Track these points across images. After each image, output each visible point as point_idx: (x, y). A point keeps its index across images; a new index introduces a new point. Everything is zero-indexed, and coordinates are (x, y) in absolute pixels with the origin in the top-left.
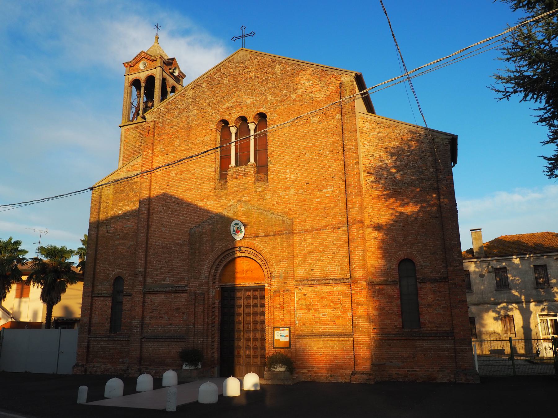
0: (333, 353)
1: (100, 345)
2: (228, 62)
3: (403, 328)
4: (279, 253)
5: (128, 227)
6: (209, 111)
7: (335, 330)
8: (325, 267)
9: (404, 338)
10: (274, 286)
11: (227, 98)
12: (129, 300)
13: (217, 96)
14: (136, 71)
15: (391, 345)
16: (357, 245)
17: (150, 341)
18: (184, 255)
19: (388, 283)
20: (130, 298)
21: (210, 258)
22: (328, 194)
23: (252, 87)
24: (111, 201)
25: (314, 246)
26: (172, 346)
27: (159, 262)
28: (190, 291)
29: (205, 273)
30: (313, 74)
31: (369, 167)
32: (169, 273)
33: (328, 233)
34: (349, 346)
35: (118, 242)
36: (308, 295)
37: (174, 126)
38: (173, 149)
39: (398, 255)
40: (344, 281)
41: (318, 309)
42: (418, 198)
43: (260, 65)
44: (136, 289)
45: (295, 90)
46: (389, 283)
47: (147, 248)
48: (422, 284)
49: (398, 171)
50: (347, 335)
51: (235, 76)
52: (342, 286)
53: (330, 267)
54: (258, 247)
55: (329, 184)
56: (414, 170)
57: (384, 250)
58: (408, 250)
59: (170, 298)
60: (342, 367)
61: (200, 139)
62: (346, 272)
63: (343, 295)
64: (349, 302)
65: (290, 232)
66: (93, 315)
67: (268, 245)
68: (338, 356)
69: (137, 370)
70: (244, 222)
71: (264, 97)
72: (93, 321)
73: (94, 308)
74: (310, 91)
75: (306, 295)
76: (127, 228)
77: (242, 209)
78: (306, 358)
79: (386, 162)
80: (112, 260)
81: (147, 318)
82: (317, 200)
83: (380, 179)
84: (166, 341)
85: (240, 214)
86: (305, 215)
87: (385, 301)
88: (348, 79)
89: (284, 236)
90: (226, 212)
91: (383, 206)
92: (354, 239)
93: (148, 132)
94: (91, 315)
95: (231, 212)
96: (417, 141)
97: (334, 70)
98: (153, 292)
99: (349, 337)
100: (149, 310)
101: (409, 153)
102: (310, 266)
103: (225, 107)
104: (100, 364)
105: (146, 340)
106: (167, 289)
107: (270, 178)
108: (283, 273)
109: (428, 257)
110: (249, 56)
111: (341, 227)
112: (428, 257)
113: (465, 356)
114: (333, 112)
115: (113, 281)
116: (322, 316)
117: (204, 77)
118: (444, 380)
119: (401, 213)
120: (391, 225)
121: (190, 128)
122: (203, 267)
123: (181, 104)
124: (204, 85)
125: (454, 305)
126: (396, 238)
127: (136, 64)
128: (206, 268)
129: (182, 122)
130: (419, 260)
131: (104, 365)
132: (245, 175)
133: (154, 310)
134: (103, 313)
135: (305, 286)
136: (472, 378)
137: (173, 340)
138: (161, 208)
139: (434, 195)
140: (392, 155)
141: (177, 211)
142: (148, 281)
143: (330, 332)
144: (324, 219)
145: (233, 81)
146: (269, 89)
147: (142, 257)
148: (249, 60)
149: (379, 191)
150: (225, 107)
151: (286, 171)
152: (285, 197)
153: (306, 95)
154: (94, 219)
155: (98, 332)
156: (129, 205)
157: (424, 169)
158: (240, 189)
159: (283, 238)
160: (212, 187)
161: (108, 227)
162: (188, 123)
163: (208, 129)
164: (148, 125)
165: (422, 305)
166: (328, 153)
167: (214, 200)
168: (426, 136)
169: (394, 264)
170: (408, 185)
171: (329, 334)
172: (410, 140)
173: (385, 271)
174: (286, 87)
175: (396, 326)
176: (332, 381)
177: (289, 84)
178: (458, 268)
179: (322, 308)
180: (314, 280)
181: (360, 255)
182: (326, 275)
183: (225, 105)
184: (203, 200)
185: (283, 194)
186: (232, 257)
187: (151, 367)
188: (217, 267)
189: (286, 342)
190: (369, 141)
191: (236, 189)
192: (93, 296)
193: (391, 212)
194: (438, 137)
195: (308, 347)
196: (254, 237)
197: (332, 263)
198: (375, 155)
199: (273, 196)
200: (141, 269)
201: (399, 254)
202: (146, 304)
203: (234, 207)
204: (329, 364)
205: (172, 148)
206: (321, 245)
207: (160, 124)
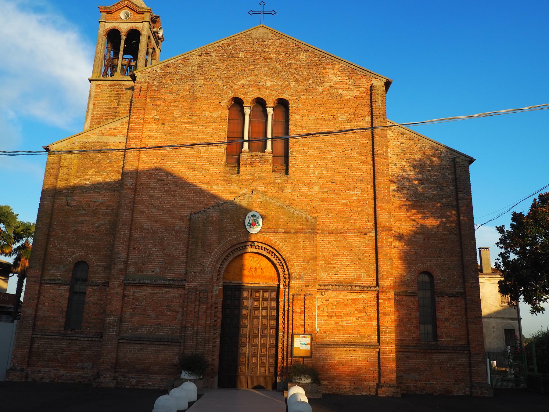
0: (356, 363)
1: (49, 344)
2: (245, 36)
4: (301, 252)
5: (98, 202)
6: (220, 84)
7: (359, 340)
8: (349, 273)
9: (422, 351)
10: (294, 288)
13: (231, 70)
15: (408, 357)
16: (386, 253)
17: (130, 343)
18: (181, 244)
19: (408, 294)
20: (97, 289)
22: (356, 196)
24: (75, 167)
26: (161, 350)
27: (147, 248)
28: (189, 286)
29: (209, 267)
30: (342, 70)
31: (392, 175)
32: (159, 263)
33: (354, 238)
34: (373, 357)
35: (82, 219)
36: (330, 300)
37: (174, 92)
39: (417, 267)
40: (371, 289)
41: (341, 316)
42: (438, 213)
43: (282, 47)
44: (114, 279)
45: (322, 82)
46: (409, 294)
48: (440, 297)
49: (420, 184)
50: (373, 345)
51: (253, 52)
52: (368, 294)
53: (355, 274)
54: (277, 244)
55: (357, 186)
56: (435, 186)
57: (404, 261)
58: (428, 263)
59: (159, 293)
60: (365, 379)
61: (207, 114)
62: (372, 279)
63: (368, 303)
64: (374, 311)
65: (313, 232)
66: (40, 306)
67: (287, 243)
68: (361, 368)
69: (112, 378)
70: (263, 215)
71: (287, 83)
72: (40, 313)
73: (42, 297)
74: (338, 87)
75: (328, 300)
76: (97, 203)
77: (258, 200)
78: (327, 369)
79: (409, 173)
80: (72, 240)
81: (127, 315)
82: (343, 201)
83: (402, 189)
84: (154, 344)
85: (255, 205)
87: (404, 312)
88: (379, 83)
89: (307, 235)
90: (239, 201)
91: (405, 216)
92: (383, 247)
93: (140, 94)
94: (37, 306)
95: (245, 201)
96: (439, 157)
97: (364, 72)
98: (137, 285)
99: (376, 347)
100: (130, 305)
101: (430, 168)
102: (334, 270)
103: (239, 83)
104: (47, 369)
105: (125, 341)
106: (158, 282)
107: (292, 171)
108: (305, 275)
109: (446, 272)
110: (270, 35)
111: (369, 232)
112: (446, 272)
113: (479, 370)
114: (362, 114)
115: (72, 266)
116: (346, 325)
117: (215, 45)
118: (460, 393)
119: (422, 225)
120: (412, 236)
121: (194, 99)
122: (207, 260)
123: (184, 69)
124: (214, 54)
125: (471, 320)
126: (415, 250)
127: (115, 11)
128: (211, 261)
129: (184, 90)
130: (438, 273)
131: (54, 370)
133: (137, 305)
134: (56, 304)
135: (329, 291)
136: (487, 392)
137: (162, 343)
138: (152, 185)
139: (454, 212)
140: (414, 167)
141: (173, 191)
142: (130, 270)
143: (354, 342)
144: (350, 222)
145: (251, 58)
146: (292, 75)
147: (125, 241)
148: (269, 39)
149: (401, 200)
150: (239, 83)
151: (309, 166)
152: (308, 193)
153: (334, 90)
154: (50, 185)
155: (46, 328)
156: (100, 176)
157: (444, 185)
158: (255, 177)
159: (305, 237)
160: (220, 171)
161: (68, 198)
162: (193, 93)
163: (217, 105)
164: (140, 85)
165: (440, 319)
167: (223, 185)
168: (447, 155)
169: (414, 276)
170: (429, 199)
171: (353, 344)
172: (432, 156)
173: (404, 282)
174: (311, 77)
175: (414, 338)
176: (356, 393)
177: (316, 75)
179: (346, 316)
181: (389, 263)
182: (351, 281)
183: (239, 81)
184: (208, 183)
185: (305, 190)
186: (242, 252)
187: (130, 375)
188: (223, 262)
189: (307, 350)
190: (392, 149)
191: (250, 177)
192: (42, 282)
193: (412, 223)
194: (459, 157)
196: (271, 232)
197: (358, 269)
198: (398, 165)
199: (294, 190)
200: (121, 254)
201: (419, 266)
202: (126, 298)
203: (249, 196)
204: (351, 376)
205: (170, 117)
206: (346, 249)
207: (154, 87)
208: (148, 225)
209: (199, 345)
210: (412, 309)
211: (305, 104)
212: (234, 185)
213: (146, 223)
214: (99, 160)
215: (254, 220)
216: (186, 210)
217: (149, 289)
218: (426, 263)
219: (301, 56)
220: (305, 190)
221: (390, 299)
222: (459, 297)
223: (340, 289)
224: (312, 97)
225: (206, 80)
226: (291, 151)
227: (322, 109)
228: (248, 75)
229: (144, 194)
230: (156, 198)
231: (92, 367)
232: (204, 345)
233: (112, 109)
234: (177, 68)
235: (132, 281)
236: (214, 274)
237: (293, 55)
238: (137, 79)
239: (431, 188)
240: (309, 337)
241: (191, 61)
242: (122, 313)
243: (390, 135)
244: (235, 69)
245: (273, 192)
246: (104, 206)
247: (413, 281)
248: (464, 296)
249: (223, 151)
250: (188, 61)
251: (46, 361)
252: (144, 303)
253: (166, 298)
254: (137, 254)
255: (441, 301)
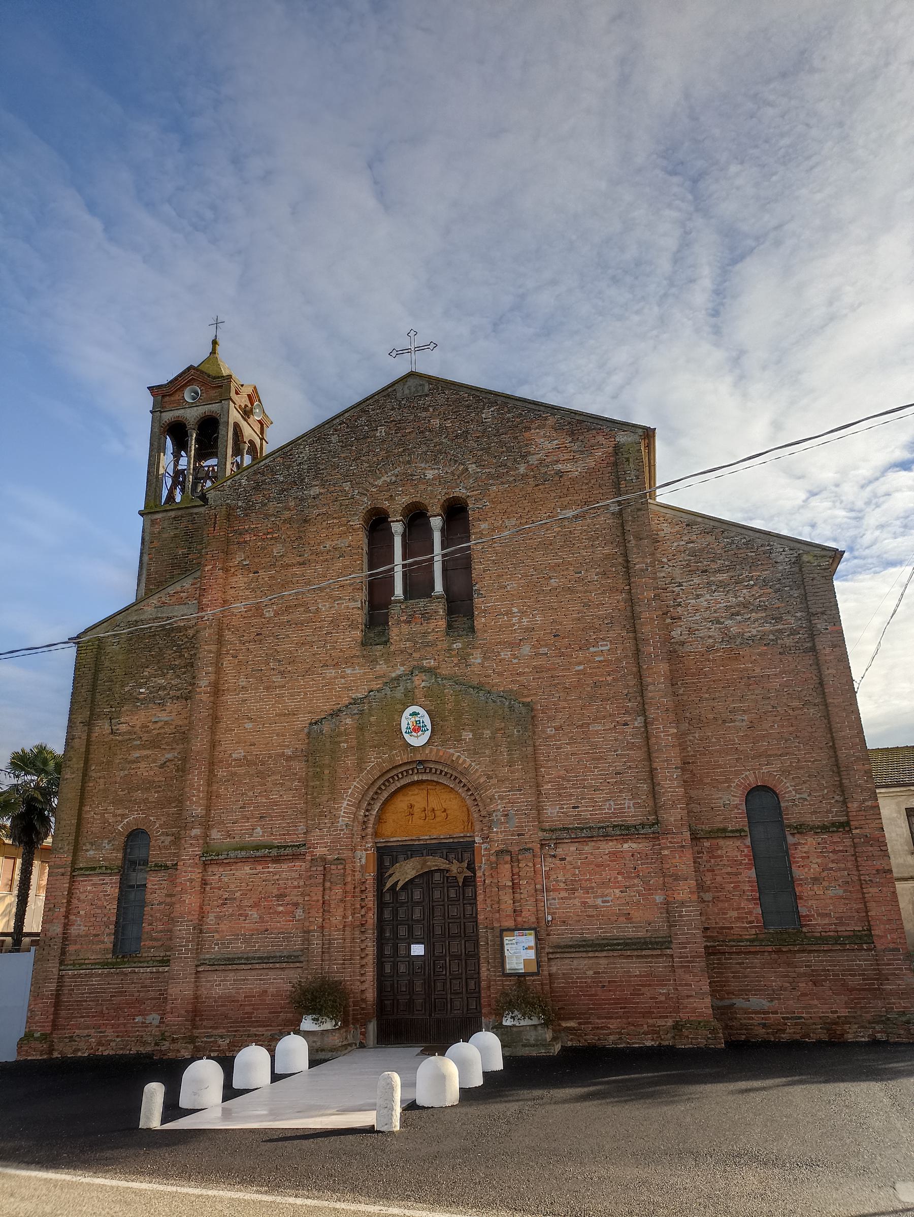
3: (765, 926)
6: (347, 489)
8: (600, 802)
11: (383, 465)
12: (162, 880)
14: (175, 405)
15: (743, 963)
16: (667, 757)
21: (355, 783)
22: (600, 656)
23: (435, 446)
25: (577, 758)
29: (345, 817)
35: (136, 754)
36: (568, 859)
37: (271, 516)
38: (268, 562)
41: (592, 888)
45: (524, 457)
47: (212, 764)
48: (797, 836)
52: (640, 841)
54: (460, 762)
56: (764, 614)
58: (764, 768)
59: (263, 873)
62: (646, 811)
66: (72, 917)
68: (640, 990)
72: (73, 931)
73: (75, 901)
75: (564, 859)
76: (160, 724)
77: (423, 684)
82: (577, 668)
86: (556, 697)
88: (629, 439)
98: (225, 861)
101: (752, 583)
103: (379, 482)
112: (804, 782)
116: (602, 904)
117: (335, 422)
128: (348, 805)
132: (426, 616)
138: (243, 681)
141: (279, 687)
146: (471, 452)
147: (200, 785)
148: (427, 395)
150: (379, 482)
156: (163, 675)
165: (801, 880)
166: (596, 577)
175: (751, 922)
176: (633, 1043)
178: (869, 803)
180: (582, 829)
181: (675, 777)
185: (507, 655)
188: (369, 804)
194: (808, 553)
195: (574, 972)
199: (485, 658)
200: (197, 810)
205: (267, 560)
206: (591, 757)
208: (239, 753)
209: (334, 964)
210: (741, 864)
211: (496, 499)
212: (381, 663)
213: (236, 750)
214: (159, 648)
215: (416, 721)
216: (301, 717)
217: (245, 868)
218: (759, 769)
219: (484, 416)
220: (507, 655)
221: (683, 847)
222: (837, 831)
223: (583, 835)
224: (507, 486)
225: (323, 485)
226: (476, 588)
227: (526, 504)
228: (393, 465)
229: (230, 698)
230: (250, 703)
231: (160, 1023)
232: (344, 964)
233: (180, 558)
234: (274, 473)
235: (215, 856)
236: (355, 829)
237: (469, 415)
238: (211, 502)
239: (756, 620)
240: (530, 934)
241: (297, 456)
242: (202, 915)
243: (665, 531)
244: (370, 457)
245: (451, 667)
246: (171, 727)
247: (736, 807)
248: (847, 829)
249: (359, 606)
250: (291, 457)
251: (83, 1017)
252: (238, 894)
253: (273, 880)
254: (223, 805)
255: (799, 844)
